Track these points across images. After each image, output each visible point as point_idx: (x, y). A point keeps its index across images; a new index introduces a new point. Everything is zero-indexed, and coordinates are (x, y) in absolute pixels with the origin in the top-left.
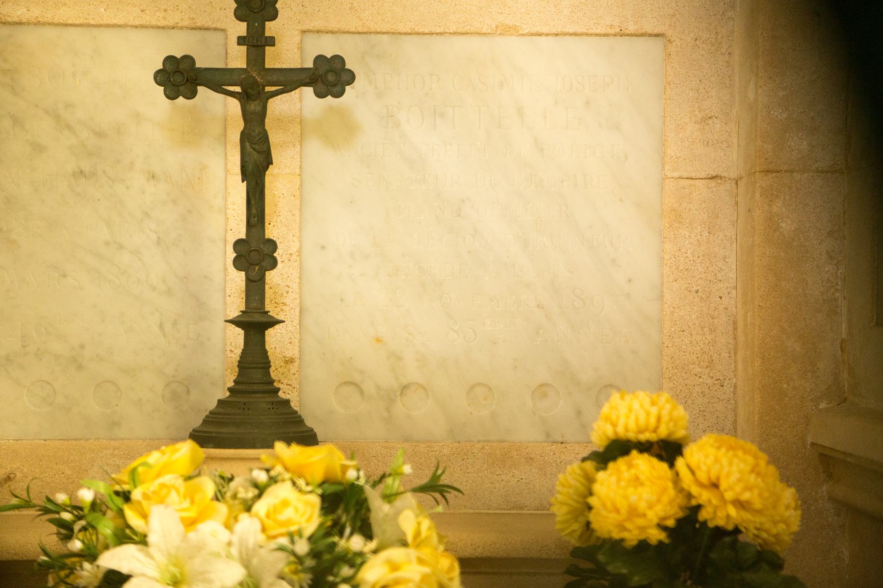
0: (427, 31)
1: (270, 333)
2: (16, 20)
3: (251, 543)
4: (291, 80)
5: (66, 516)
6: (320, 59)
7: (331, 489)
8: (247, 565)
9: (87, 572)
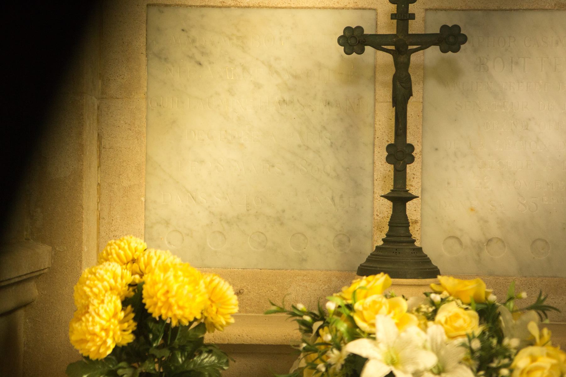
0: (508, 8)
1: (409, 205)
2: (246, 5)
3: (439, 340)
4: (425, 41)
5: (307, 318)
6: (444, 28)
7: (481, 307)
8: (437, 353)
9: (334, 355)
